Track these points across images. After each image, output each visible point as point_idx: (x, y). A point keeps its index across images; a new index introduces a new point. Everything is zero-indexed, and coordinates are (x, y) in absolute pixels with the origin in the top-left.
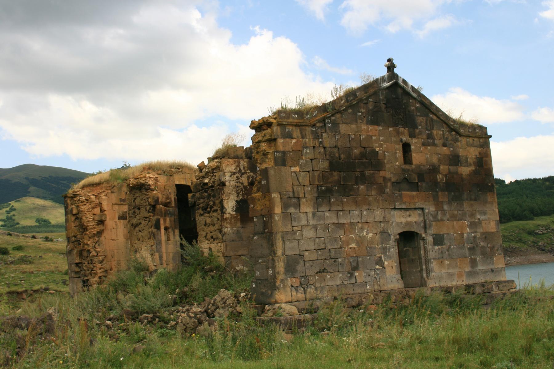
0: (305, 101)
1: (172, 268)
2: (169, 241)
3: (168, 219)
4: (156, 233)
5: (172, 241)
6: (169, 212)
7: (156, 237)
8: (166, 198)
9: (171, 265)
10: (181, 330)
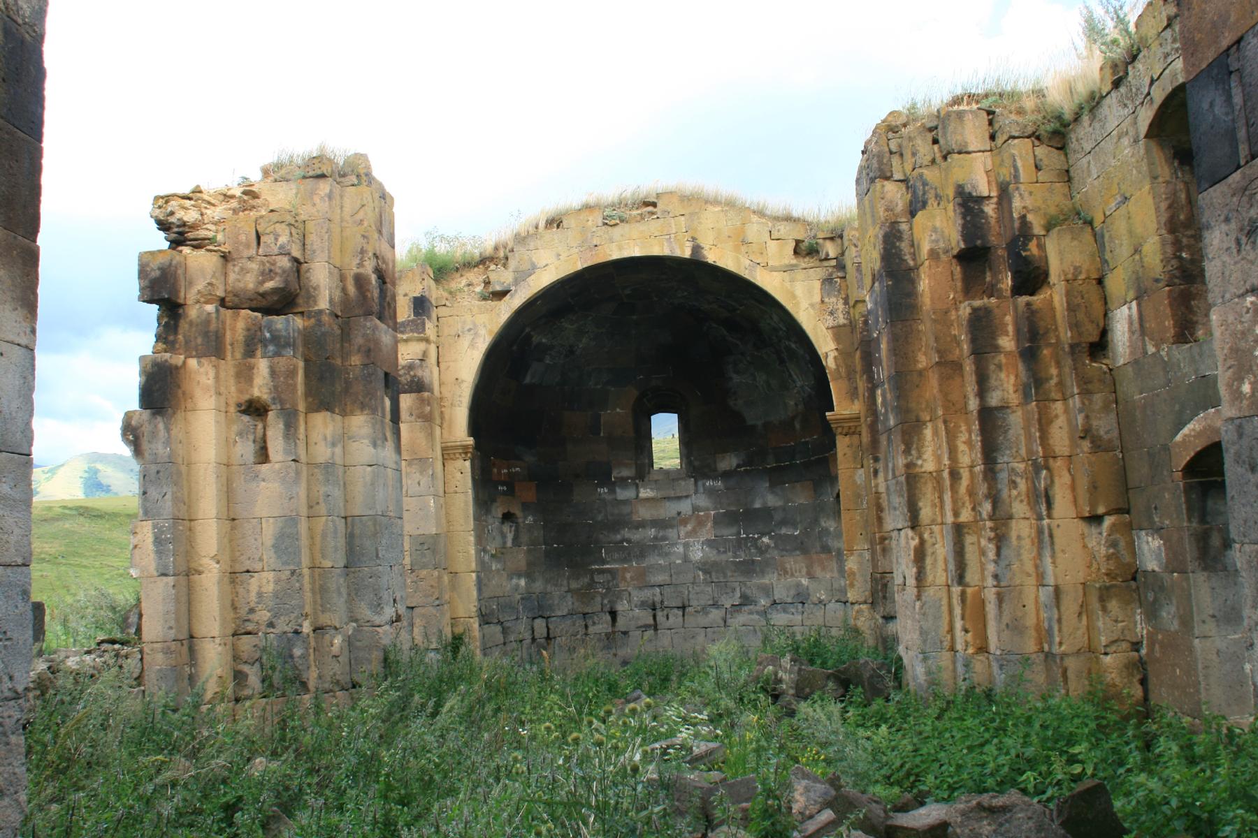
0: (1020, 83)
1: (269, 588)
2: (265, 467)
3: (262, 366)
4: (147, 429)
5: (277, 466)
6: (268, 335)
7: (145, 445)
8: (263, 273)
9: (264, 574)
10: (925, 184)
